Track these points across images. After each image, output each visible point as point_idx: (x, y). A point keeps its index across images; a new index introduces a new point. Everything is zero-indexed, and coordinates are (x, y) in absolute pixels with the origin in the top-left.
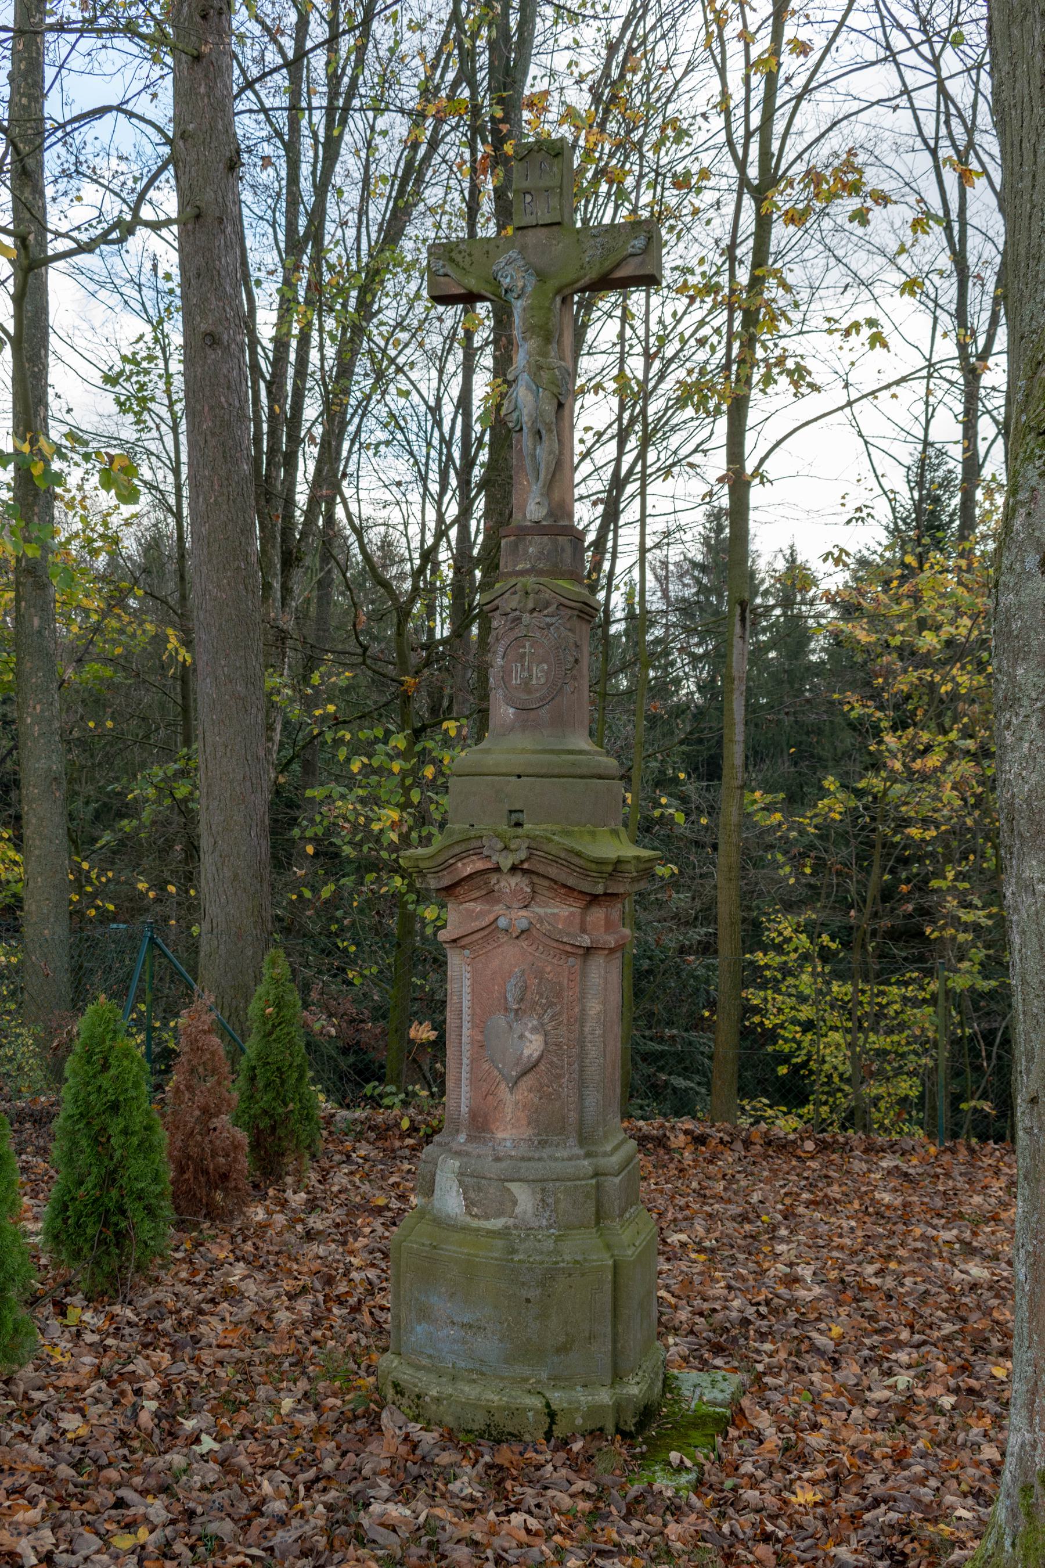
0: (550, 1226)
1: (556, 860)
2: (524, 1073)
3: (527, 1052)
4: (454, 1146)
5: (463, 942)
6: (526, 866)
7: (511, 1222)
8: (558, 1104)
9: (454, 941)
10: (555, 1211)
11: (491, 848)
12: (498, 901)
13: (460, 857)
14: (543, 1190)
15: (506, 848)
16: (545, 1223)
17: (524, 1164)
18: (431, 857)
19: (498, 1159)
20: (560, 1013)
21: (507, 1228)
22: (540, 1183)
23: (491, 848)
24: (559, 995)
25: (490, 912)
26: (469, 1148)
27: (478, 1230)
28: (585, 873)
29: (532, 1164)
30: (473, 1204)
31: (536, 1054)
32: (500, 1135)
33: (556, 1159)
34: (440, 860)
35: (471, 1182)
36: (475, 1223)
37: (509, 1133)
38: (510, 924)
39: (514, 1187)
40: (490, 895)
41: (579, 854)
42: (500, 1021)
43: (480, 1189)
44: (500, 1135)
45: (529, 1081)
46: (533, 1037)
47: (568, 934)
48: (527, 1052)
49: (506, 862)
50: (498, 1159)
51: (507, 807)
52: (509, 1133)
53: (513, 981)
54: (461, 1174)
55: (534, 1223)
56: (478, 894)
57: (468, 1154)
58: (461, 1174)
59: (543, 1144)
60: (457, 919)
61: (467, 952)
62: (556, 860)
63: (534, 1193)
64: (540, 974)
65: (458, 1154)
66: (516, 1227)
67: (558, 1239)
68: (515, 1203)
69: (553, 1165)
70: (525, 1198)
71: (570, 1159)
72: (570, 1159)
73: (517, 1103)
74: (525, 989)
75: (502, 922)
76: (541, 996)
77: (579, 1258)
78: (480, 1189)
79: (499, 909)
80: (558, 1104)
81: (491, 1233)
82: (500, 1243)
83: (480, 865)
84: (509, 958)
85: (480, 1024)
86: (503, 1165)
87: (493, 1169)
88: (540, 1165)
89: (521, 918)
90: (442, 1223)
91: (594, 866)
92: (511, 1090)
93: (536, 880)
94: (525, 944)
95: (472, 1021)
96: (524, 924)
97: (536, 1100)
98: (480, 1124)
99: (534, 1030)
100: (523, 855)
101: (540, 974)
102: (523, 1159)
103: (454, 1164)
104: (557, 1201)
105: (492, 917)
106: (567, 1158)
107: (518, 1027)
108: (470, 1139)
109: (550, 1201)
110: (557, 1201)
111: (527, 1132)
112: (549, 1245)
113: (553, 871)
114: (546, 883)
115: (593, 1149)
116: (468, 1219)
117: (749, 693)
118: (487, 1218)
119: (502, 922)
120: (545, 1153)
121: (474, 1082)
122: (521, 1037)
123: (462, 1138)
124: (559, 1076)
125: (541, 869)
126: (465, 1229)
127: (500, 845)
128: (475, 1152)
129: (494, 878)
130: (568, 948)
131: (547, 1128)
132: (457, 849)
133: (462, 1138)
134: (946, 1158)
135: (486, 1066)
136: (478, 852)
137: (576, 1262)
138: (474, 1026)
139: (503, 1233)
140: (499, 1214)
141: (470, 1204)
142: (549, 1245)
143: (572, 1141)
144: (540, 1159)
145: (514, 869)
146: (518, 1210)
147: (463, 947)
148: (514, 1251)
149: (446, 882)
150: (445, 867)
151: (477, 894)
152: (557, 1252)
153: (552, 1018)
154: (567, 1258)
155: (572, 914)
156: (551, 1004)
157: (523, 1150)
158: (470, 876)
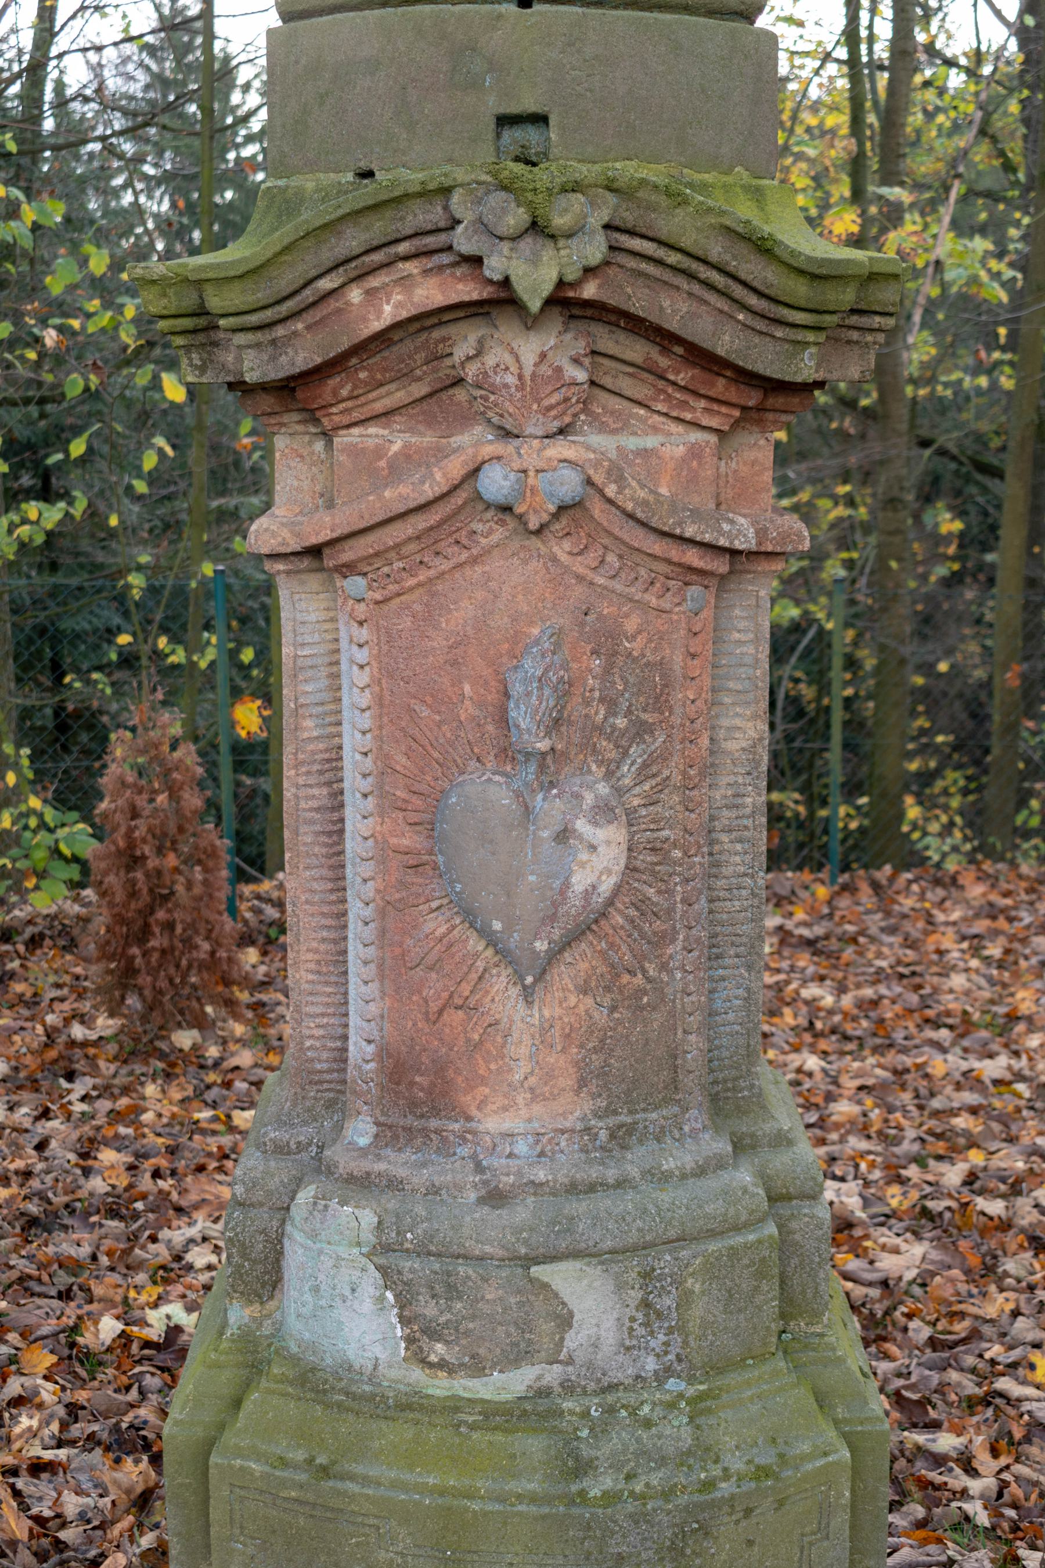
0: (666, 1372)
1: (691, 268)
2: (567, 943)
3: (580, 881)
4: (345, 1163)
5: (348, 554)
6: (590, 291)
7: (552, 1375)
8: (658, 1018)
9: (315, 552)
10: (681, 1328)
11: (482, 225)
12: (464, 419)
13: (357, 267)
14: (647, 1275)
15: (536, 227)
16: (651, 1364)
17: (579, 1206)
18: (254, 273)
19: (495, 1197)
20: (664, 757)
21: (544, 1393)
22: (638, 1259)
23: (482, 225)
24: (660, 702)
25: (441, 454)
26: (396, 1163)
27: (454, 1406)
28: (770, 312)
29: (604, 1202)
30: (433, 1333)
31: (607, 886)
32: (491, 1124)
33: (665, 1178)
34: (286, 279)
35: (419, 1274)
36: (440, 1386)
37: (523, 1113)
38: (522, 490)
39: (563, 1278)
40: (446, 395)
41: (764, 248)
42: (489, 790)
43: (453, 1291)
44: (491, 1124)
45: (582, 960)
46: (599, 835)
47: (696, 514)
48: (580, 881)
49: (535, 275)
50: (495, 1197)
51: (494, 105)
52: (523, 1113)
53: (532, 666)
54: (382, 1248)
55: (622, 1370)
56: (399, 396)
57: (394, 1185)
58: (384, 1252)
59: (622, 1137)
60: (299, 490)
61: (356, 584)
62: (691, 268)
63: (620, 1287)
64: (607, 643)
65: (360, 1185)
66: (568, 1388)
67: (699, 1408)
68: (565, 1321)
69: (665, 1197)
70: (593, 1306)
71: (701, 1171)
72: (701, 1171)
73: (545, 1029)
74: (565, 690)
75: (495, 483)
76: (611, 704)
77: (767, 1458)
78: (453, 1291)
79: (473, 441)
80: (658, 1018)
81: (499, 1416)
82: (534, 1445)
83: (431, 292)
84: (509, 596)
85: (421, 803)
86: (522, 1213)
87: (492, 1230)
88: (627, 1202)
89: (550, 466)
90: (320, 1385)
91: (800, 290)
92: (528, 995)
93: (610, 341)
94: (561, 550)
95: (380, 792)
96: (567, 484)
97: (601, 1017)
98: (421, 1094)
99: (603, 812)
100: (594, 250)
101: (607, 643)
102: (573, 1189)
103: (361, 1218)
104: (685, 1300)
105: (455, 468)
106: (692, 1173)
107: (550, 809)
108: (388, 1135)
109: (668, 1302)
110: (685, 1300)
111: (576, 1109)
112: (677, 1431)
113: (674, 309)
114: (637, 350)
115: (744, 1127)
116: (417, 1375)
117: (194, 251)
118: (478, 1368)
119: (495, 483)
120: (634, 1162)
121: (396, 970)
122: (564, 835)
123: (361, 1131)
124: (665, 938)
125: (638, 300)
126: (411, 1405)
127: (516, 218)
128: (421, 1178)
129: (464, 341)
130: (693, 557)
131: (635, 1085)
132: (353, 240)
133: (361, 1131)
134: (844, 902)
135: (436, 925)
136: (432, 247)
137: (763, 1472)
138: (388, 804)
139: (534, 1411)
140: (517, 1356)
141: (419, 1334)
142: (677, 1431)
143: (695, 1118)
144: (622, 1184)
145: (563, 303)
146: (573, 1340)
147: (347, 569)
148: (582, 1468)
149: (301, 357)
150: (305, 303)
151: (397, 395)
152: (703, 1451)
153: (644, 773)
154: (737, 1464)
155: (695, 452)
156: (641, 730)
157: (568, 1163)
158: (383, 338)
